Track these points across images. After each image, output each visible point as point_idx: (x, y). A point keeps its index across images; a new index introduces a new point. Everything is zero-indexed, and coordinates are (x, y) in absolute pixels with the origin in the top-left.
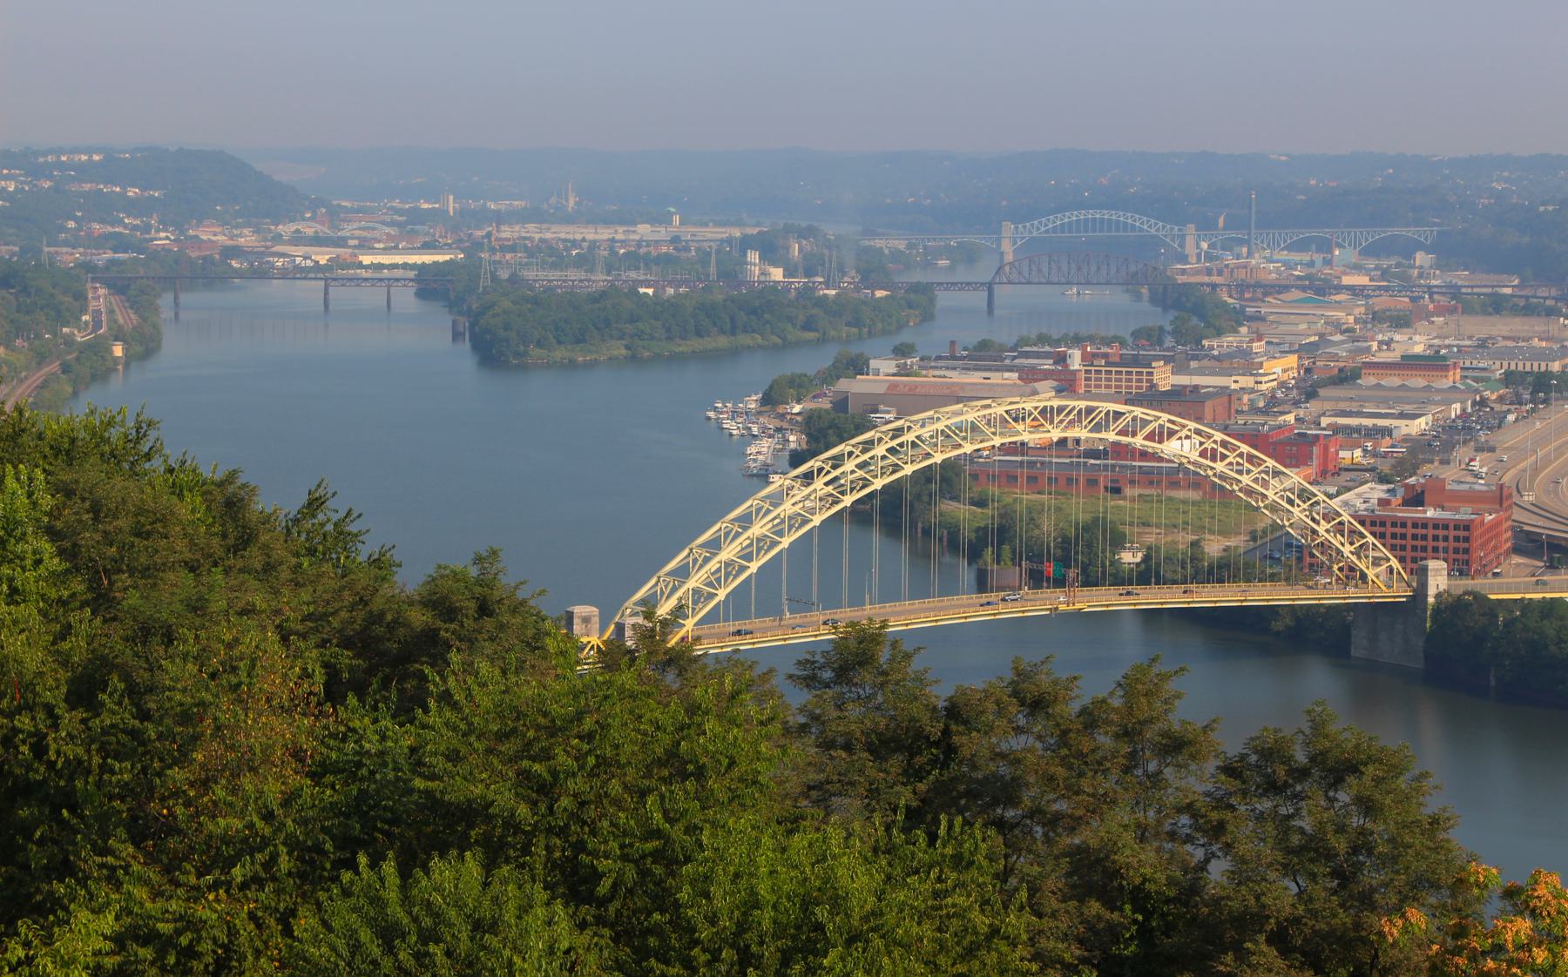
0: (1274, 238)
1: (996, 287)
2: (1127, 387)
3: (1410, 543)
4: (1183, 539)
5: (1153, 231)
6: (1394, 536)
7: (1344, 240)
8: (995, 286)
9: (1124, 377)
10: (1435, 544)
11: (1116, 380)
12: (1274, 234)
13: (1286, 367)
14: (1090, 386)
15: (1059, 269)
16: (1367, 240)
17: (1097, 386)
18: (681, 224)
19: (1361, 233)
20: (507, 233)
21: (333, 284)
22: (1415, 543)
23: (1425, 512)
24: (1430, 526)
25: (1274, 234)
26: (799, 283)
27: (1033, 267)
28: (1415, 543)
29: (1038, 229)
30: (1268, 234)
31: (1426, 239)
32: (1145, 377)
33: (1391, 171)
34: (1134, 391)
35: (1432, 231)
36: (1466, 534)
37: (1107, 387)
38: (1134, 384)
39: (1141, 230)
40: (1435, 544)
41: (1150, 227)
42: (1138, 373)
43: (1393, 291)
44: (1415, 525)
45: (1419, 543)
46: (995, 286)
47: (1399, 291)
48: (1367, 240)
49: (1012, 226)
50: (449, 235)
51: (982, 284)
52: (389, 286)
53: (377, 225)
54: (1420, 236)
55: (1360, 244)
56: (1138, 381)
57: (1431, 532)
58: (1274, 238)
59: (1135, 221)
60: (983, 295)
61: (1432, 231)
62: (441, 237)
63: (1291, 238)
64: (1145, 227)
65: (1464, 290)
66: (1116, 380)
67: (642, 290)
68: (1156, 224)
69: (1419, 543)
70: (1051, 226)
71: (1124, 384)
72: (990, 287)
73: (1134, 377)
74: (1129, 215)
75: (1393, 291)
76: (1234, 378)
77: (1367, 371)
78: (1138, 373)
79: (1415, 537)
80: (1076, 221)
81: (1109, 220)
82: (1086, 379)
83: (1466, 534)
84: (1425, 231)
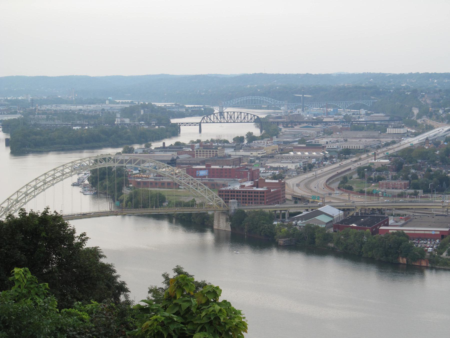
0: (344, 104)
2: (206, 156)
3: (247, 198)
6: (226, 195)
8: (201, 124)
12: (344, 103)
13: (273, 149)
14: (198, 156)
15: (217, 118)
16: (350, 104)
17: (200, 156)
18: (109, 103)
20: (44, 108)
22: (249, 198)
24: (259, 193)
25: (344, 103)
26: (133, 124)
27: (215, 117)
28: (249, 198)
29: (232, 103)
30: (342, 103)
31: (368, 104)
32: (205, 152)
34: (208, 157)
35: (370, 102)
36: (220, 194)
38: (208, 155)
42: (210, 151)
44: (249, 192)
45: (250, 198)
46: (201, 124)
49: (223, 103)
51: (197, 123)
56: (210, 154)
57: (230, 194)
58: (344, 104)
59: (261, 98)
62: (18, 110)
63: (350, 104)
64: (270, 102)
65: (353, 122)
66: (201, 154)
68: (233, 101)
69: (250, 198)
76: (252, 153)
77: (295, 150)
78: (210, 151)
79: (249, 196)
80: (243, 101)
81: (257, 100)
82: (196, 153)
83: (220, 194)
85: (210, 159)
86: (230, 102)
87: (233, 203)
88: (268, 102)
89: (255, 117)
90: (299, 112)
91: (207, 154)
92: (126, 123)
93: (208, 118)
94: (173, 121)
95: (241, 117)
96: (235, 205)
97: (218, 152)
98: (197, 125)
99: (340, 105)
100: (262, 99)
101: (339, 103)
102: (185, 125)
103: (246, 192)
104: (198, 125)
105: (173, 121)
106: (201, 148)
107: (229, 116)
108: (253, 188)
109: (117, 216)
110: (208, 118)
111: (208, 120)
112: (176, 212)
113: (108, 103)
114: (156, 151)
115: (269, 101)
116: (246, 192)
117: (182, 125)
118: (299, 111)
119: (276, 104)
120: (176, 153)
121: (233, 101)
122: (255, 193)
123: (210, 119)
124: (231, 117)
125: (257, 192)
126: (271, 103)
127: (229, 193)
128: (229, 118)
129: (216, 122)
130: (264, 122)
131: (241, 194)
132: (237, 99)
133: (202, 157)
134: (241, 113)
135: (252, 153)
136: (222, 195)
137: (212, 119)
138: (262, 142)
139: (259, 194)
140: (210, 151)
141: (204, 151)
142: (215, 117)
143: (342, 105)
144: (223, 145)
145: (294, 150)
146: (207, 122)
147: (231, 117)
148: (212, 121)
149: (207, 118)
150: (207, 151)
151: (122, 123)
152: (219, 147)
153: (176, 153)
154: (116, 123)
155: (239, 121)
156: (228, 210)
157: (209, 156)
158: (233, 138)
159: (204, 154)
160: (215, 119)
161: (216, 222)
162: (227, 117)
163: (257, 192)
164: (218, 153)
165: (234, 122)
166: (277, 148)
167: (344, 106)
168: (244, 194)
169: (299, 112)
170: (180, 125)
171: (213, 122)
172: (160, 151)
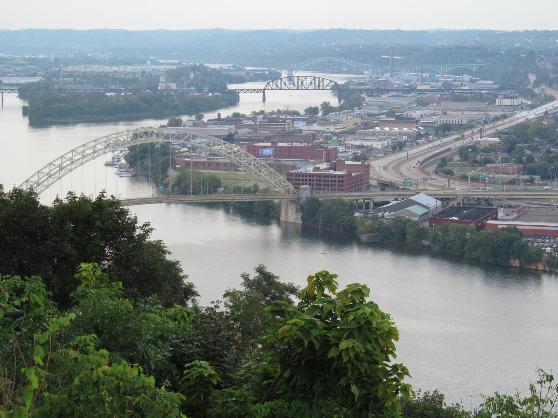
3: (322, 183)
4: (252, 183)
6: (295, 180)
7: (400, 69)
9: (274, 126)
10: (301, 180)
11: (271, 128)
16: (450, 68)
17: (264, 130)
19: (410, 67)
21: (5, 92)
23: (329, 172)
27: (283, 83)
29: (304, 66)
31: (473, 69)
34: (274, 132)
37: (268, 131)
39: (349, 65)
40: (301, 180)
42: (271, 125)
44: (325, 177)
47: (438, 92)
48: (450, 68)
49: (293, 65)
50: (43, 70)
51: (261, 90)
52: (2, 93)
53: (12, 66)
54: (471, 68)
55: (445, 72)
56: (276, 128)
58: (443, 68)
60: (261, 95)
62: (39, 71)
64: (351, 65)
65: (455, 91)
66: (271, 128)
67: (107, 94)
70: (313, 63)
71: (274, 129)
72: (264, 91)
73: (278, 127)
74: (340, 58)
76: (328, 127)
78: (271, 125)
86: (302, 64)
91: (273, 128)
93: (274, 84)
95: (315, 83)
100: (341, 61)
102: (251, 92)
105: (231, 87)
108: (329, 172)
109: (161, 204)
110: (274, 84)
111: (274, 87)
114: (210, 124)
115: (346, 62)
116: (321, 176)
120: (234, 126)
121: (305, 63)
123: (277, 85)
124: (302, 83)
126: (352, 66)
128: (300, 84)
131: (323, 179)
133: (266, 132)
135: (328, 127)
137: (279, 85)
139: (337, 179)
142: (283, 83)
145: (380, 124)
146: (272, 89)
147: (302, 83)
149: (273, 84)
151: (167, 88)
153: (234, 126)
155: (321, 88)
159: (269, 128)
160: (283, 85)
162: (298, 83)
166: (360, 122)
169: (386, 78)
170: (239, 93)
171: (281, 89)
172: (214, 124)
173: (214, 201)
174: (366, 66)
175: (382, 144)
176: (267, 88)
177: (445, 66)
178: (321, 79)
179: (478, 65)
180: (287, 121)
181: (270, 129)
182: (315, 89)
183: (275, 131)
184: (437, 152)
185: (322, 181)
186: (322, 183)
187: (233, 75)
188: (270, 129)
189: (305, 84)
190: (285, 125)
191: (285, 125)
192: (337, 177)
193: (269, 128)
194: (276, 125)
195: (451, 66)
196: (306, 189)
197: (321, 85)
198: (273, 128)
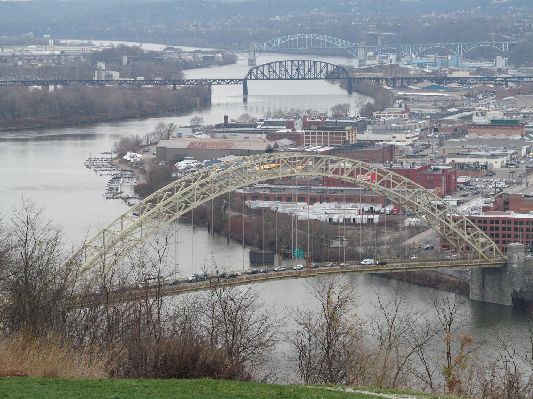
1: (249, 82)
3: (500, 232)
5: (340, 46)
9: (329, 136)
12: (412, 47)
16: (471, 47)
19: (415, 47)
24: (500, 222)
25: (412, 47)
27: (271, 70)
29: (271, 45)
30: (456, 45)
33: (479, 7)
35: (505, 44)
39: (333, 45)
41: (333, 41)
42: (331, 134)
43: (484, 81)
46: (248, 81)
49: (256, 44)
51: (240, 80)
55: (463, 52)
56: (338, 138)
58: (460, 48)
60: (241, 87)
61: (505, 44)
63: (471, 47)
64: (335, 44)
65: (508, 79)
68: (272, 42)
72: (245, 82)
73: (335, 136)
75: (484, 81)
76: (394, 135)
78: (331, 134)
79: (504, 229)
84: (501, 44)
85: (338, 148)
86: (268, 43)
87: (516, 250)
88: (332, 44)
89: (327, 68)
90: (391, 62)
91: (327, 138)
92: (114, 78)
93: (259, 72)
94: (191, 75)
95: (315, 70)
96: (520, 253)
97: (347, 134)
98: (239, 83)
99: (453, 50)
100: (321, 39)
101: (404, 47)
102: (236, 83)
103: (486, 221)
104: (242, 83)
105: (191, 75)
106: (314, 129)
107: (294, 68)
108: (510, 214)
109: (299, 279)
110: (259, 72)
112: (409, 268)
113: (52, 45)
114: (217, 132)
117: (213, 83)
118: (391, 60)
119: (346, 47)
120: (265, 135)
122: (505, 223)
123: (263, 73)
124: (298, 70)
125: (508, 221)
127: (527, 228)
129: (272, 78)
130: (354, 79)
131: (501, 225)
132: (279, 38)
134: (315, 62)
135: (394, 135)
136: (497, 235)
137: (266, 73)
138: (393, 115)
139: (512, 226)
140: (332, 134)
141: (322, 133)
142: (271, 70)
143: (409, 51)
144: (335, 121)
146: (257, 79)
147: (298, 70)
148: (266, 76)
149: (257, 71)
150: (326, 134)
151: (107, 79)
152: (346, 126)
153: (265, 135)
154: (96, 79)
155: (312, 77)
156: (505, 264)
157: (337, 142)
158: (331, 107)
159: (321, 138)
160: (283, 72)
161: (477, 286)
162: (292, 70)
163: (508, 221)
164: (347, 136)
165: (304, 78)
167: (460, 52)
168: (507, 226)
169: (391, 62)
170: (211, 84)
171: (268, 79)
173: (393, 271)
174: (356, 45)
175: (502, 162)
176: (249, 78)
177: (464, 45)
178: (323, 64)
179: (508, 43)
180: (347, 128)
181: (323, 140)
182: (315, 78)
183: (337, 142)
184: (60, 134)
185: (501, 229)
186: (500, 232)
187: (174, 58)
188: (323, 140)
189: (301, 71)
190: (345, 134)
191: (345, 134)
192: (525, 222)
193: (321, 138)
194: (332, 134)
195: (472, 45)
196: (518, 249)
197: (313, 72)
198: (333, 138)
